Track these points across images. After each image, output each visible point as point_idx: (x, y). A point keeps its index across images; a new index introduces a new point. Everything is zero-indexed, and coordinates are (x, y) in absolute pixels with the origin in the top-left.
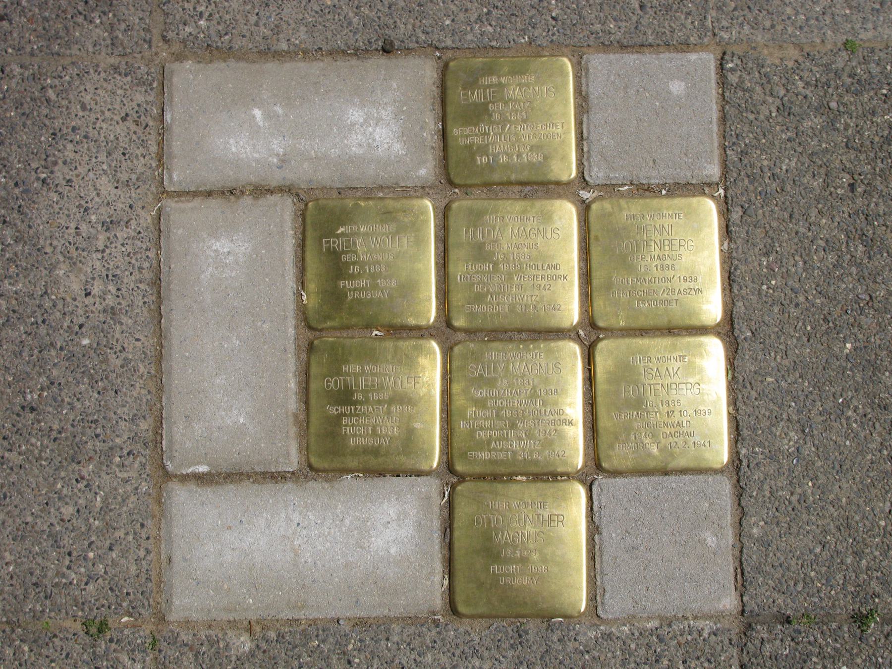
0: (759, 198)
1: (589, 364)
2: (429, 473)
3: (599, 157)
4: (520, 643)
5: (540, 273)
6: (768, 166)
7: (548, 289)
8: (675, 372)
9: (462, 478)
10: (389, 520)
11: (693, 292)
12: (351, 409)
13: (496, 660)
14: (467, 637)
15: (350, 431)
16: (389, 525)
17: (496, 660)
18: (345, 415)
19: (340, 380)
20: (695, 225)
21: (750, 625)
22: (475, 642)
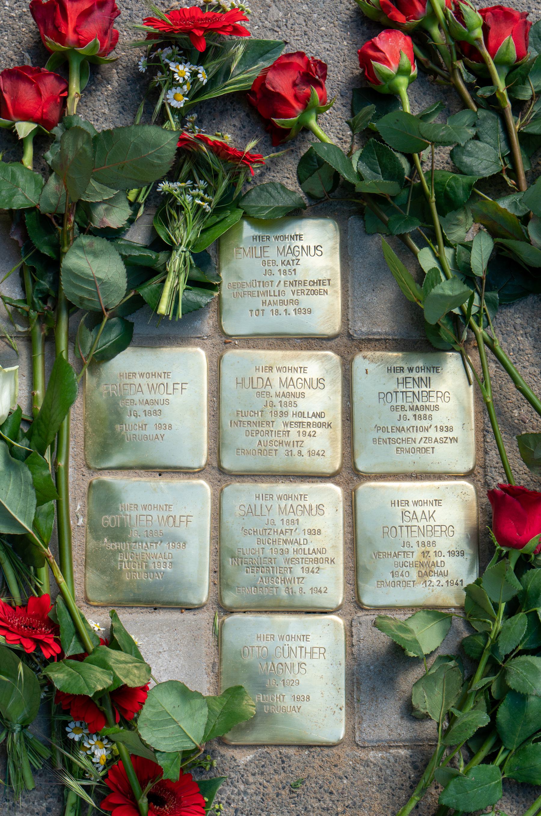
0: (511, 354)
1: (145, 603)
2: (199, 608)
3: (363, 312)
4: (283, 768)
5: (305, 420)
6: (521, 324)
7: (325, 592)
8: (430, 515)
9: (229, 611)
10: (161, 651)
11: (448, 440)
12: (126, 546)
13: (260, 784)
14: (233, 762)
15: (125, 567)
16: (161, 655)
17: (260, 784)
18: (120, 551)
19: (117, 518)
20: (133, 727)
21: (51, 171)
22: (241, 767)
